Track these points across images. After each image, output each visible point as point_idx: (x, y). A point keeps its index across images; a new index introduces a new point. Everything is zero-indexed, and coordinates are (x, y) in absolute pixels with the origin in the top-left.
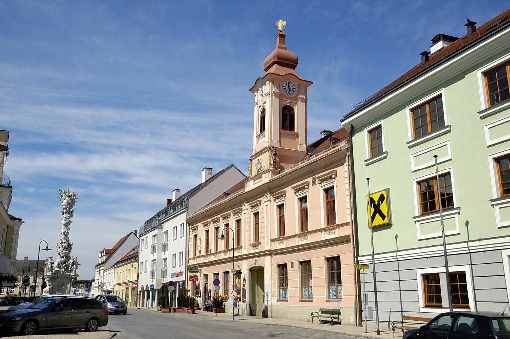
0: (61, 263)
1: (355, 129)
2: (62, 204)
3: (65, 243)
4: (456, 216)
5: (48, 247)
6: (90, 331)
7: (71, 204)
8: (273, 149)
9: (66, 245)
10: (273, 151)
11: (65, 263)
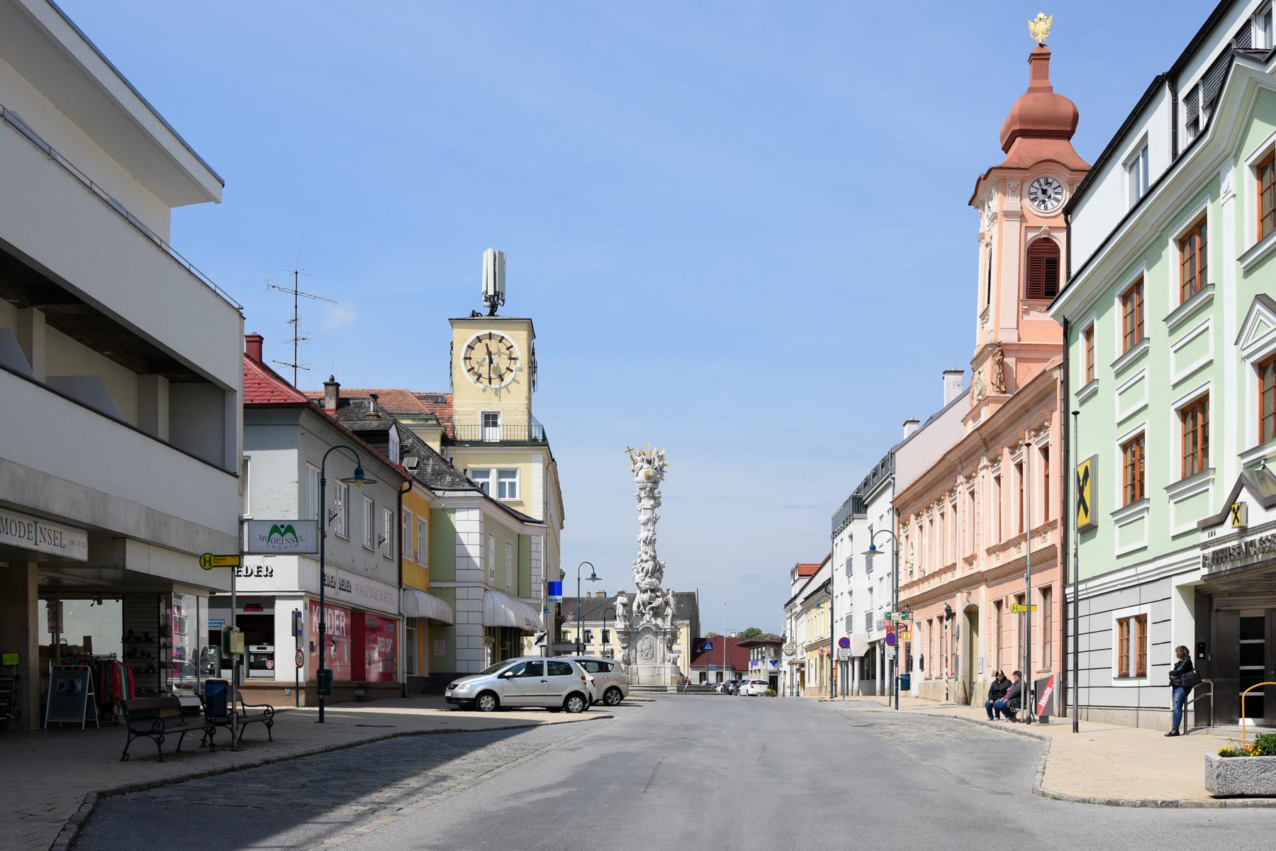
0: (643, 604)
1: (1072, 323)
2: (637, 479)
3: (646, 561)
4: (1145, 514)
5: (594, 575)
6: (571, 712)
7: (654, 481)
8: (998, 349)
9: (649, 565)
10: (997, 353)
11: (651, 603)
